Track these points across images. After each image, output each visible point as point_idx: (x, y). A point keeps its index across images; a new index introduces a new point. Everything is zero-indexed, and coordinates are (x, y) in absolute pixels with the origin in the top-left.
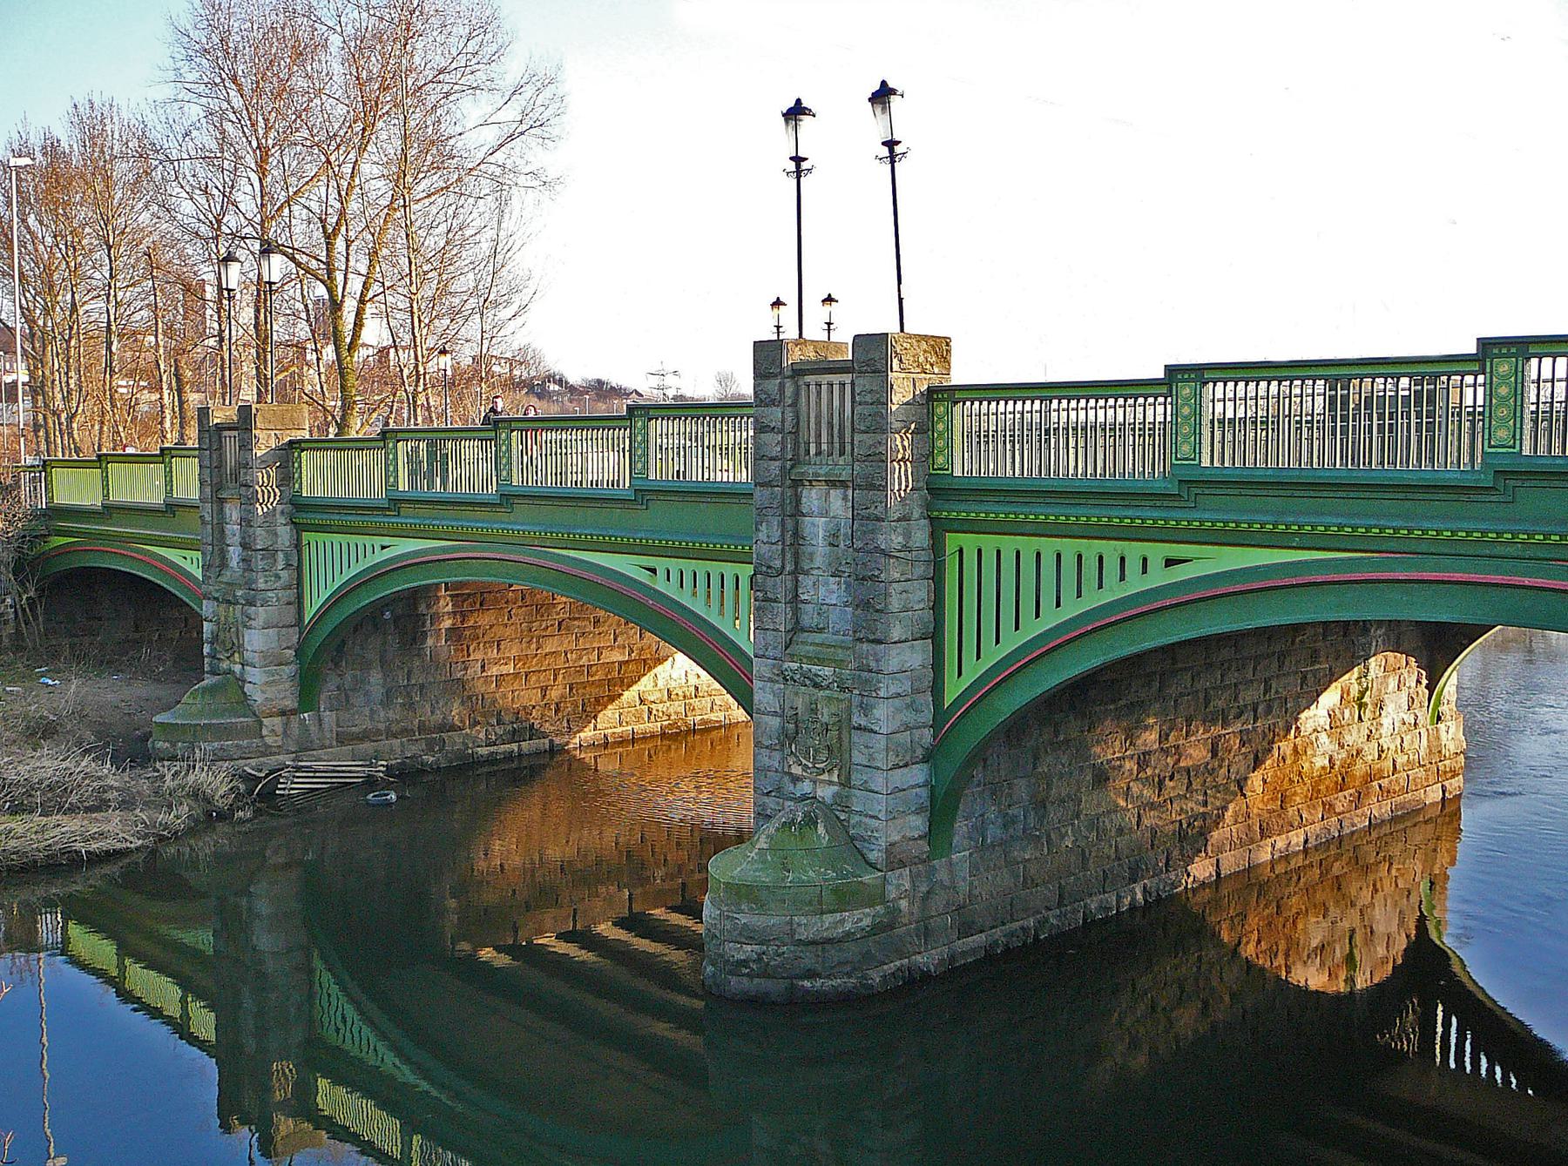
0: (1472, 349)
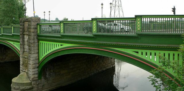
0: (91, 20)
